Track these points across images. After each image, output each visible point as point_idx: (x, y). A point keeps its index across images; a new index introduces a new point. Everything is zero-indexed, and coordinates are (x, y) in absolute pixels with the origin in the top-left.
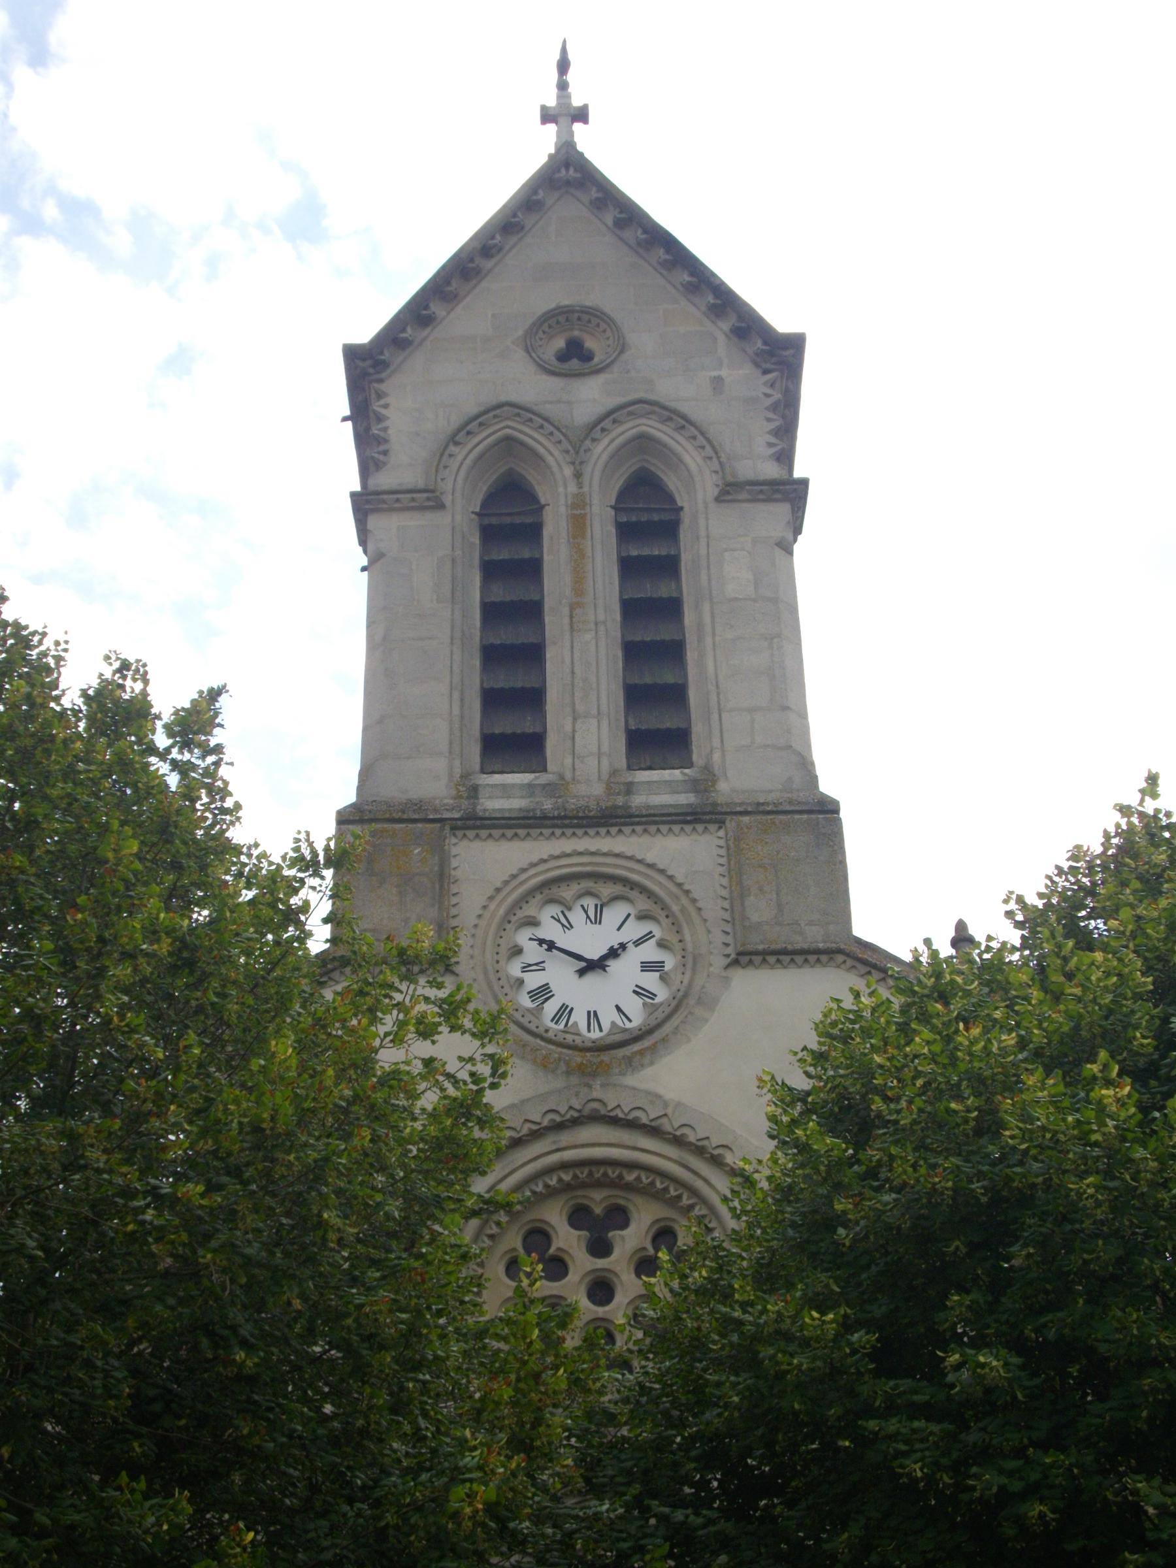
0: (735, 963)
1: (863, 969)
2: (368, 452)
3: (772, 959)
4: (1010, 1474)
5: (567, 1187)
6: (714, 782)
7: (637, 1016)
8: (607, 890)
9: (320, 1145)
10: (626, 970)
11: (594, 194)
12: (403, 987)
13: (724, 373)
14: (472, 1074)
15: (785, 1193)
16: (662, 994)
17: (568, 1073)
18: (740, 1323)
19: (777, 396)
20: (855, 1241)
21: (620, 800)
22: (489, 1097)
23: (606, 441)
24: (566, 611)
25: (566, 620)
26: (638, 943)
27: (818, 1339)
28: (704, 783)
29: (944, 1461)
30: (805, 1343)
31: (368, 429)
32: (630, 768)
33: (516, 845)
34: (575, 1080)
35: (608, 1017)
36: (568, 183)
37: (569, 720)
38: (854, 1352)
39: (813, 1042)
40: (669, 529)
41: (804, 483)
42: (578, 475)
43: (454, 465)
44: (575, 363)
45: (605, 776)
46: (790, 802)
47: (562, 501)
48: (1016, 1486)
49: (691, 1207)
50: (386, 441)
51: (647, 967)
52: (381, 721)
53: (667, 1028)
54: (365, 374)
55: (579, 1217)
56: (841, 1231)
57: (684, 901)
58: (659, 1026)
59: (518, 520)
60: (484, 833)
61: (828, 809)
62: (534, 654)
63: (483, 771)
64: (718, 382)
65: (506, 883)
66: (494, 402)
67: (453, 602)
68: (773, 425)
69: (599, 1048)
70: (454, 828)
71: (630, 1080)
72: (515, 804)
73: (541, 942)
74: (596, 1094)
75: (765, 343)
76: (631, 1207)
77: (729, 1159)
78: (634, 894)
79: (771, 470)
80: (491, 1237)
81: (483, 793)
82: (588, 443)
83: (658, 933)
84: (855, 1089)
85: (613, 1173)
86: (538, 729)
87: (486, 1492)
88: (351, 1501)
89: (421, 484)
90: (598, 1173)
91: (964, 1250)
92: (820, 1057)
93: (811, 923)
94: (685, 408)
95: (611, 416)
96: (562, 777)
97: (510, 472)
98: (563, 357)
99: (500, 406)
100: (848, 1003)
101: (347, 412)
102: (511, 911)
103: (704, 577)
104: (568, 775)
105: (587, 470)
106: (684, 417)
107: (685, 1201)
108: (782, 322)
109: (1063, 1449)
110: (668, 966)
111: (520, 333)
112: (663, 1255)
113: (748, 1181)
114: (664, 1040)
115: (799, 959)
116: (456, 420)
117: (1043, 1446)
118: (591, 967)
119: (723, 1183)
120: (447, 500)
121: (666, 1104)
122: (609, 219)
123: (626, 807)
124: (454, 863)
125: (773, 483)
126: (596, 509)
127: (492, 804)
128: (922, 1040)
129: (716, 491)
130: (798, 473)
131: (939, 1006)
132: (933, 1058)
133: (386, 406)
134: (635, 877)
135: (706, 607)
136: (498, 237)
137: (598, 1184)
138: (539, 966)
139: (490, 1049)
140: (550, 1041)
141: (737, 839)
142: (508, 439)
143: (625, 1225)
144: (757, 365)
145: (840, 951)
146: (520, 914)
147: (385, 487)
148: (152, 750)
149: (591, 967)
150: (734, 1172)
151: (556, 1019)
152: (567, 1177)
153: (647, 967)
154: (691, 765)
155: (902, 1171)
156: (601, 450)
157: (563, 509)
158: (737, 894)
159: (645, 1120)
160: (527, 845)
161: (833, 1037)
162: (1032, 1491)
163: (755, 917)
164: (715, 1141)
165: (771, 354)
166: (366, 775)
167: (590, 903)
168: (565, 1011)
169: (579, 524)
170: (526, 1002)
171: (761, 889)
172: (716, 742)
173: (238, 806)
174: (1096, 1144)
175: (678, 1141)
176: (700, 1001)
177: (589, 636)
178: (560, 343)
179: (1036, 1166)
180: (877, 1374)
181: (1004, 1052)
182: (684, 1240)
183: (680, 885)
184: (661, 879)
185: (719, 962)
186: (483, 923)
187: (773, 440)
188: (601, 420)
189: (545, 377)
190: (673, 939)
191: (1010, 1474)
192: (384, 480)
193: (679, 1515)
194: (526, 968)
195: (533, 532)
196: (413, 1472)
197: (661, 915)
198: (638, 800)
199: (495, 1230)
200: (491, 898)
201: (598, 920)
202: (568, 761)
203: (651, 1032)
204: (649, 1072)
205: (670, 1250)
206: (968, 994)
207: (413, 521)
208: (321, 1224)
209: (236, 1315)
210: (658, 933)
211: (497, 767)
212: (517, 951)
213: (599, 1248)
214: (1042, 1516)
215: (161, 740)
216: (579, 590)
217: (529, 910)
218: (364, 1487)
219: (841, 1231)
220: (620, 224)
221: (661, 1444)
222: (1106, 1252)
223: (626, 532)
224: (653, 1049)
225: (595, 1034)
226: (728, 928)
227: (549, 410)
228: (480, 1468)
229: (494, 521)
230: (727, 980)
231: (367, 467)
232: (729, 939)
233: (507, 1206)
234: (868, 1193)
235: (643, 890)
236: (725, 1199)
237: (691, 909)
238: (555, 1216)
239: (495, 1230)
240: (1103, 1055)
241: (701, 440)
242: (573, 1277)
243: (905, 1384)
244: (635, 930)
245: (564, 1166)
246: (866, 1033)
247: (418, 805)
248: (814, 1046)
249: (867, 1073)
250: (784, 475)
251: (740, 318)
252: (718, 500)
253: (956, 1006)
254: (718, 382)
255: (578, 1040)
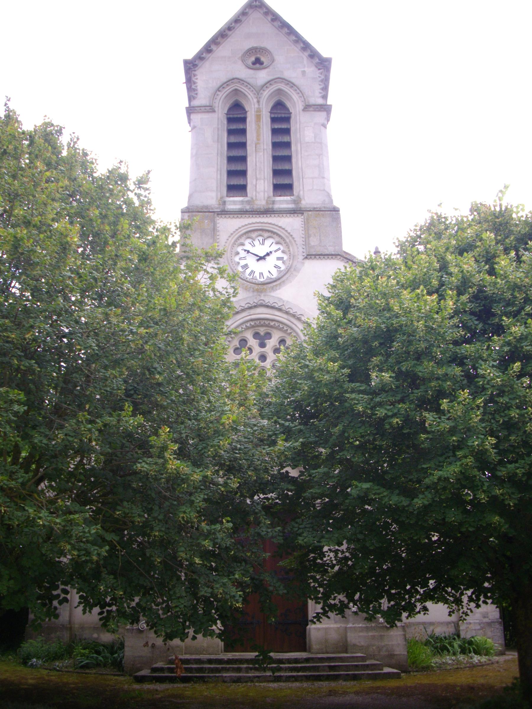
0: (306, 258)
1: (346, 261)
2: (191, 94)
3: (317, 257)
4: (388, 410)
5: (253, 327)
6: (300, 201)
7: (275, 274)
8: (266, 234)
9: (183, 315)
10: (271, 260)
11: (265, 10)
12: (206, 264)
13: (306, 69)
14: (227, 292)
15: (321, 328)
16: (283, 267)
17: (253, 291)
18: (308, 366)
19: (323, 77)
20: (344, 342)
21: (271, 206)
22: (232, 299)
23: (267, 91)
24: (254, 146)
25: (254, 149)
26: (276, 251)
27: (332, 371)
28: (297, 201)
29: (368, 406)
30: (328, 372)
31: (191, 87)
32: (274, 196)
33: (238, 220)
34: (255, 294)
35: (266, 275)
36: (256, 6)
37: (255, 180)
38: (343, 375)
39: (331, 282)
40: (287, 119)
41: (331, 106)
42: (258, 102)
43: (219, 98)
44: (258, 66)
45: (266, 198)
46: (325, 207)
47: (253, 110)
48: (390, 414)
49: (291, 333)
50: (197, 90)
51: (279, 259)
52: (195, 179)
53: (284, 278)
54: (190, 69)
55: (256, 335)
56: (340, 339)
57: (290, 238)
58: (282, 277)
59: (239, 116)
60: (227, 216)
61: (336, 210)
62: (243, 159)
63: (227, 196)
64: (304, 73)
65: (234, 232)
66: (232, 78)
67: (218, 142)
68: (321, 87)
69: (263, 284)
70: (218, 214)
71: (273, 294)
72: (237, 207)
73: (245, 250)
74: (262, 298)
75: (319, 60)
76: (272, 332)
77: (303, 318)
78: (275, 236)
79: (320, 101)
80: (229, 341)
81: (227, 203)
82: (262, 91)
83: (282, 248)
84: (345, 296)
85: (267, 322)
86: (245, 183)
87: (234, 417)
88: (190, 420)
89: (208, 104)
90: (262, 322)
91: (378, 345)
92: (334, 287)
93: (330, 246)
94: (293, 80)
95: (269, 83)
96: (252, 198)
97: (237, 101)
98: (254, 63)
99: (233, 79)
100: (343, 270)
101: (184, 81)
102: (236, 241)
103: (298, 135)
104: (254, 198)
105: (261, 100)
106: (293, 83)
107: (289, 331)
108: (325, 54)
109: (404, 403)
110: (285, 259)
111: (240, 55)
112: (282, 347)
113: (309, 325)
114: (284, 282)
115: (326, 257)
116: (219, 84)
117: (399, 402)
118: (261, 258)
119: (301, 326)
120: (216, 109)
121: (284, 301)
122: (269, 19)
123: (273, 208)
124: (218, 225)
125: (321, 105)
126: (264, 113)
127: (230, 207)
128: (367, 282)
129: (303, 108)
130: (329, 103)
131: (371, 272)
132: (370, 287)
133: (197, 79)
134: (275, 231)
135: (299, 145)
136: (233, 24)
137: (262, 326)
138: (244, 258)
139: (232, 285)
140: (247, 282)
141: (307, 219)
142: (236, 90)
143: (270, 338)
144: (316, 67)
145: (339, 255)
146: (239, 242)
147: (196, 105)
148: (129, 190)
149: (261, 258)
150: (304, 322)
151: (250, 275)
152: (252, 323)
153: (279, 259)
154: (293, 195)
155: (359, 321)
156: (266, 94)
157: (253, 113)
158: (307, 236)
159: (277, 306)
160: (242, 220)
161: (338, 280)
162: (394, 415)
163: (312, 244)
164: (299, 313)
165: (321, 63)
166: (190, 197)
167: (261, 239)
168: (252, 272)
169: (258, 117)
170: (240, 269)
171: (315, 235)
172: (301, 188)
173: (155, 209)
174: (423, 313)
175: (287, 313)
176: (295, 270)
177: (261, 154)
178: (253, 59)
179: (403, 319)
180: (349, 381)
181: (392, 286)
182: (289, 342)
183: (289, 233)
184: (284, 231)
185: (301, 258)
186: (227, 245)
187: (321, 91)
188: (266, 84)
189: (248, 70)
190: (286, 250)
191: (388, 410)
192: (195, 103)
193: (287, 424)
194: (240, 259)
195: (243, 120)
196: (210, 411)
197: (283, 242)
198: (276, 206)
199: (230, 339)
200: (230, 237)
201: (263, 244)
202: (254, 193)
203: (279, 279)
204: (278, 291)
205: (284, 346)
206: (381, 268)
207: (205, 116)
208: (182, 339)
209: (156, 365)
210: (282, 248)
211: (232, 195)
212: (238, 253)
213: (262, 345)
214: (397, 422)
215: (132, 187)
216: (258, 139)
217: (242, 241)
218: (194, 416)
219: (340, 339)
220: (273, 20)
221: (282, 404)
222: (423, 345)
223: (274, 120)
224: (280, 284)
225: (262, 280)
226: (304, 247)
227: (250, 81)
228: (230, 410)
229: (231, 116)
230: (303, 263)
231: (191, 98)
232: (304, 251)
233: (235, 333)
234: (349, 328)
235: (278, 235)
236: (302, 330)
237: (292, 241)
238: (249, 335)
239: (230, 339)
240: (422, 287)
241: (298, 91)
242: (254, 354)
243: (358, 384)
244: (275, 247)
245: (252, 320)
246: (348, 279)
247: (207, 207)
248: (332, 283)
249: (349, 292)
250: (325, 103)
251: (311, 51)
252: (303, 110)
253: (377, 272)
254: (304, 73)
255: (257, 282)
